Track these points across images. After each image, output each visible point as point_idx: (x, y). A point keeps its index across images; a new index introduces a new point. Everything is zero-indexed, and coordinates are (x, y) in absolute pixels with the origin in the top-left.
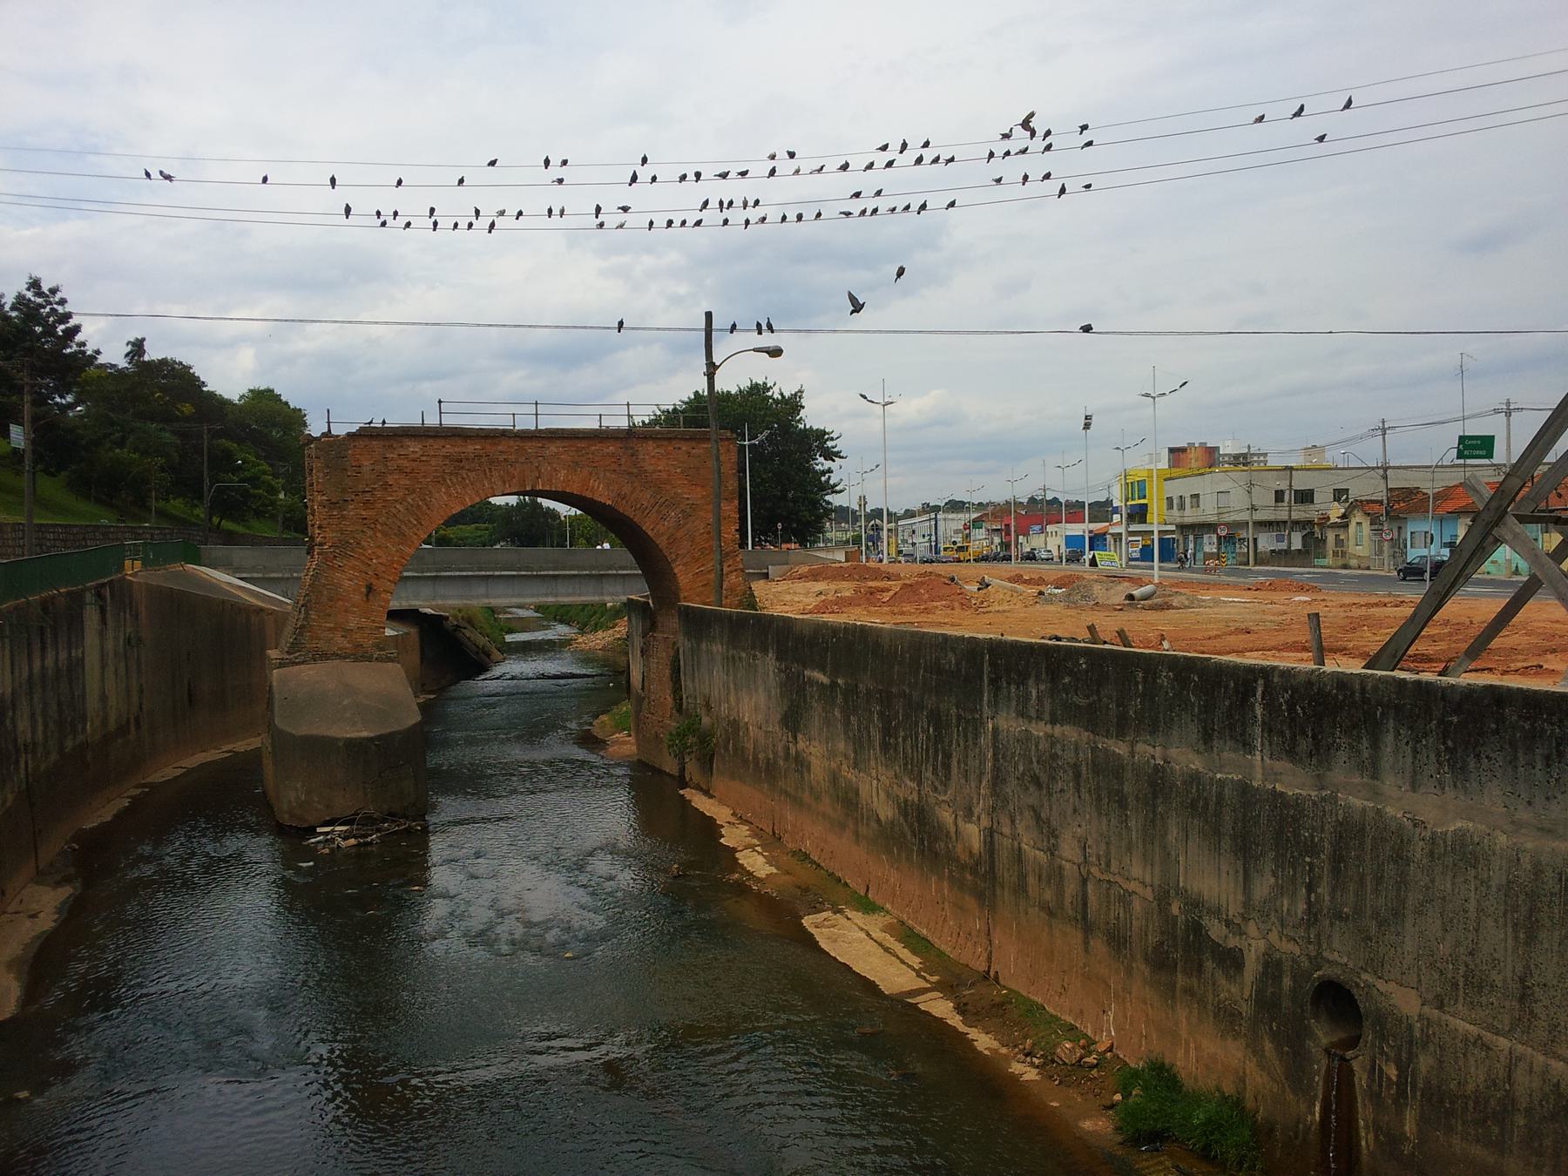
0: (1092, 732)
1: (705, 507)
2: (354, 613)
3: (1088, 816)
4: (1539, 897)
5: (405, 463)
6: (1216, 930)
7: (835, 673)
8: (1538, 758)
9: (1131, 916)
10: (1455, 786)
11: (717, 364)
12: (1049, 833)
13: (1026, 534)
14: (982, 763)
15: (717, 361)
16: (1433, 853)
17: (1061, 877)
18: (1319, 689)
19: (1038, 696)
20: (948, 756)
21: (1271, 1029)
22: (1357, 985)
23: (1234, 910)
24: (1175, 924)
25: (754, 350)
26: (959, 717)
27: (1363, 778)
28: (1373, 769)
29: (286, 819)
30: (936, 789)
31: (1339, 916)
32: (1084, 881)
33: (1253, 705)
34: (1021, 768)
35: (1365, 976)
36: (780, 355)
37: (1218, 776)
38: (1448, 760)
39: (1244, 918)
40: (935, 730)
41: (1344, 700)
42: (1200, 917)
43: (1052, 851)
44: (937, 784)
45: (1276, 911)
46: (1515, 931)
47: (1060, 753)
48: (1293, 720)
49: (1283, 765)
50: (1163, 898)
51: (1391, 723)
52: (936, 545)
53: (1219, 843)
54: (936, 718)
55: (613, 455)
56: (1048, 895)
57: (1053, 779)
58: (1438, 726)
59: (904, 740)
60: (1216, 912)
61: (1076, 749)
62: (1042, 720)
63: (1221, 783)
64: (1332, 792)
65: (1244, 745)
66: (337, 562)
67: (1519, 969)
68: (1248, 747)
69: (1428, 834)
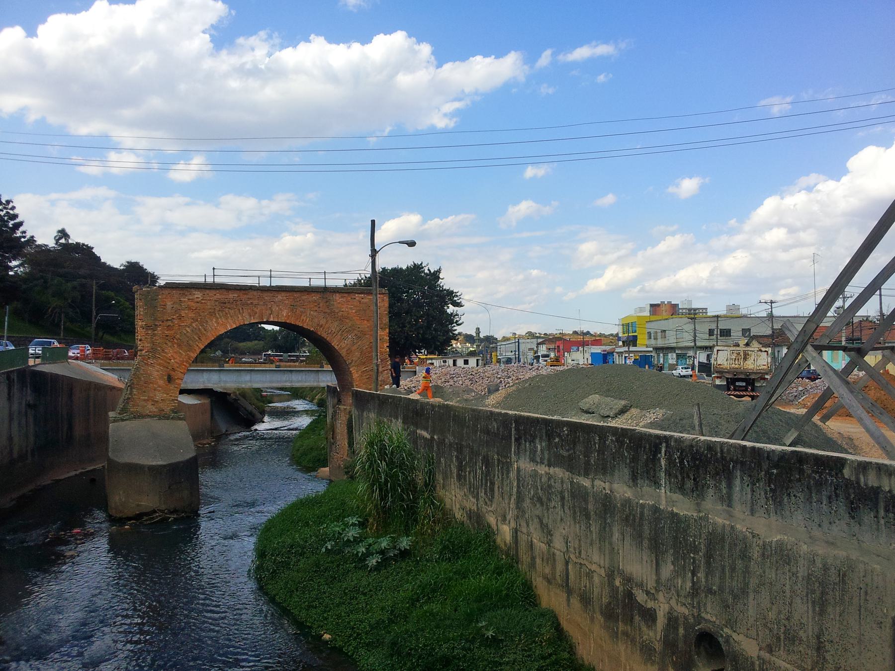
0: (571, 472)
1: (369, 333)
2: (159, 391)
3: (568, 523)
4: (826, 585)
5: (192, 304)
6: (640, 597)
7: (433, 432)
8: (824, 497)
9: (593, 585)
10: (776, 513)
11: (377, 250)
12: (548, 532)
13: (569, 352)
14: (511, 488)
15: (377, 248)
16: (764, 554)
17: (554, 560)
18: (697, 450)
19: (541, 449)
20: (492, 484)
21: (672, 659)
22: (722, 636)
23: (651, 584)
24: (618, 592)
25: (399, 242)
26: (498, 460)
27: (723, 506)
28: (728, 500)
29: (113, 512)
30: (486, 503)
31: (710, 591)
32: (567, 563)
33: (659, 459)
34: (532, 493)
35: (726, 630)
36: (414, 246)
37: (641, 501)
38: (772, 497)
39: (656, 590)
40: (486, 468)
41: (711, 458)
42: (631, 588)
43: (549, 543)
44: (487, 500)
45: (675, 587)
46: (814, 607)
47: (553, 484)
48: (682, 468)
49: (677, 496)
50: (610, 575)
51: (738, 473)
52: (519, 357)
53: (642, 543)
54: (487, 461)
55: (315, 302)
56: (547, 570)
57: (549, 500)
58: (765, 475)
59: (470, 473)
60: (641, 585)
61: (562, 482)
62: (543, 464)
63: (643, 506)
64: (706, 514)
65: (655, 483)
66: (150, 361)
67: (816, 630)
68: (656, 484)
69: (761, 543)
